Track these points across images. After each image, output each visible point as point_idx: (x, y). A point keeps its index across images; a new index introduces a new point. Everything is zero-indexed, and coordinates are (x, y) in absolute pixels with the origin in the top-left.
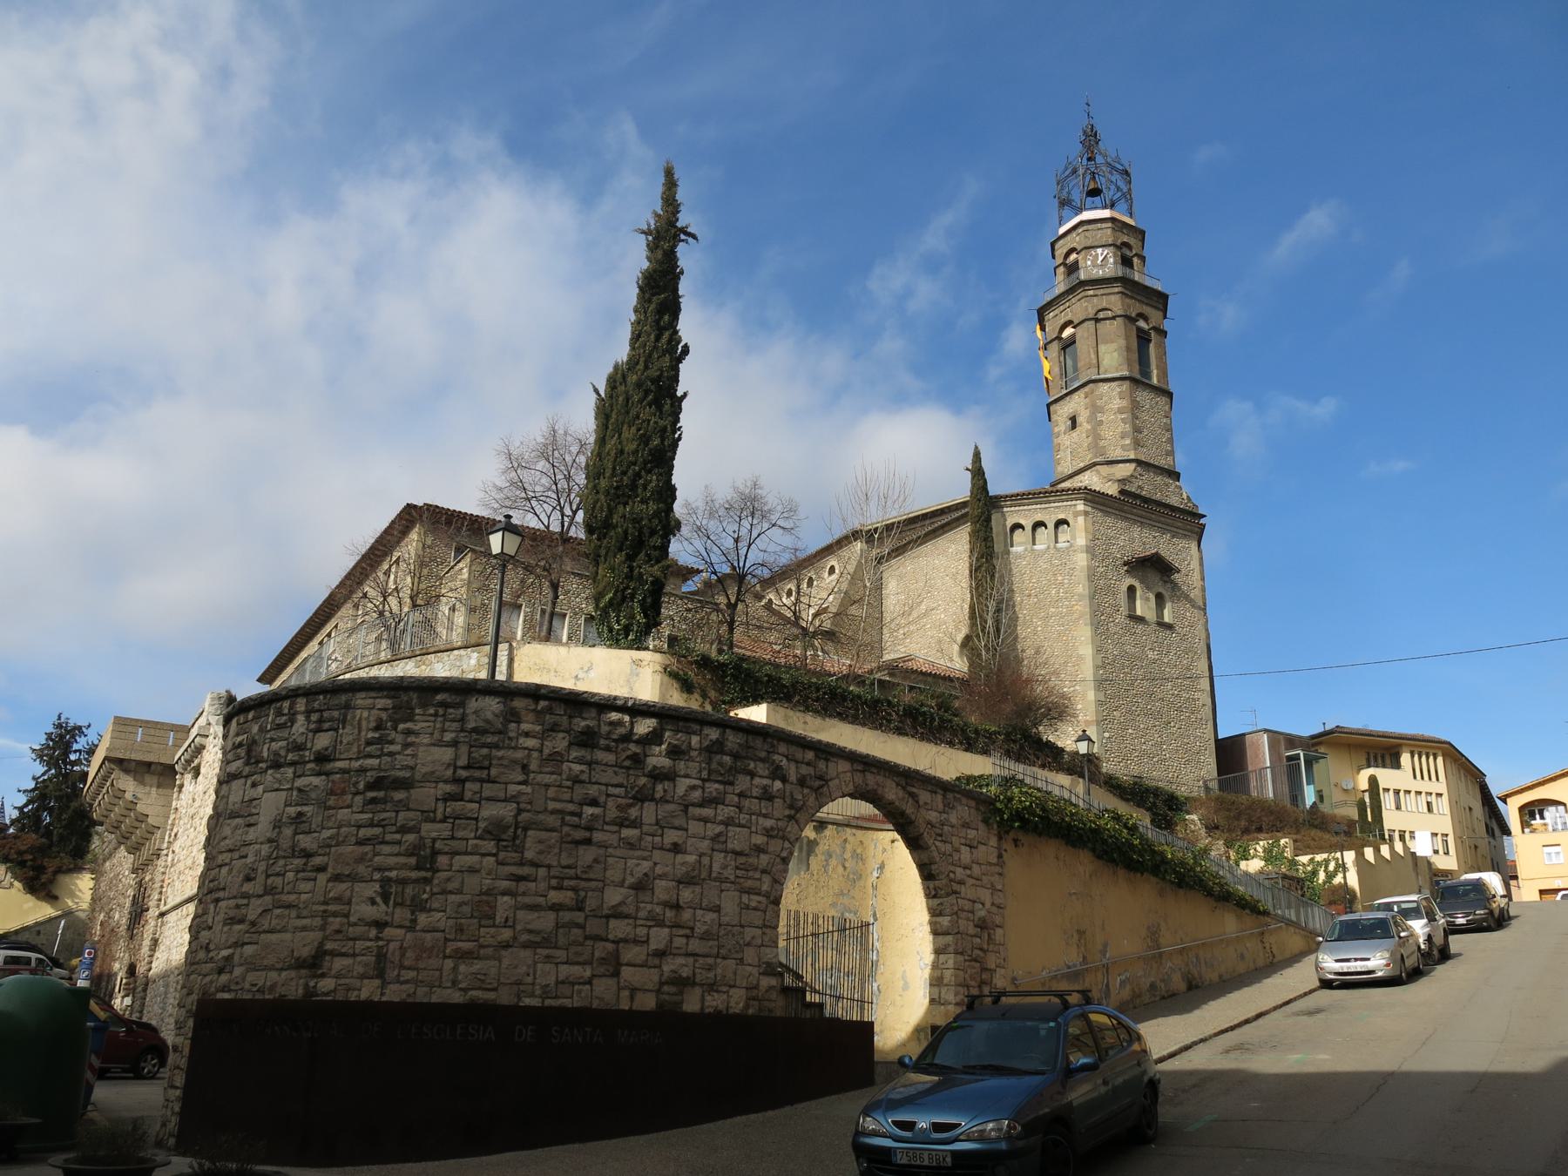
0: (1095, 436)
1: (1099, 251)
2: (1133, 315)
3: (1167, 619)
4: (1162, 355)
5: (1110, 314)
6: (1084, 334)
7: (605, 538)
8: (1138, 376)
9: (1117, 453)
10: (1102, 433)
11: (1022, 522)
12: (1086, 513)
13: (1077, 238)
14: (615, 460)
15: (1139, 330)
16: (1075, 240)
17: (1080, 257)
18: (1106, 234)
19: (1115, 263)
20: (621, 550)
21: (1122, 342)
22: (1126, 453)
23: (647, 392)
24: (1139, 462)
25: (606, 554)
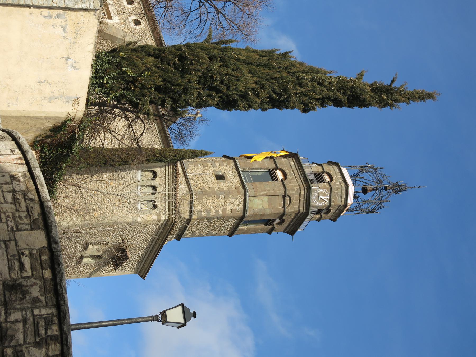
0: (211, 193)
1: (328, 197)
2: (284, 218)
3: (85, 260)
4: (256, 231)
5: (287, 204)
6: (277, 187)
7: (175, 68)
8: (245, 219)
9: (196, 208)
10: (211, 198)
11: (157, 180)
12: (159, 221)
13: (338, 183)
14: (233, 76)
15: (274, 220)
16: (337, 180)
17: (326, 184)
18: (338, 201)
19: (318, 206)
20: (164, 80)
21: (268, 211)
22: (196, 212)
23: (280, 95)
24: (188, 221)
25: (163, 69)
